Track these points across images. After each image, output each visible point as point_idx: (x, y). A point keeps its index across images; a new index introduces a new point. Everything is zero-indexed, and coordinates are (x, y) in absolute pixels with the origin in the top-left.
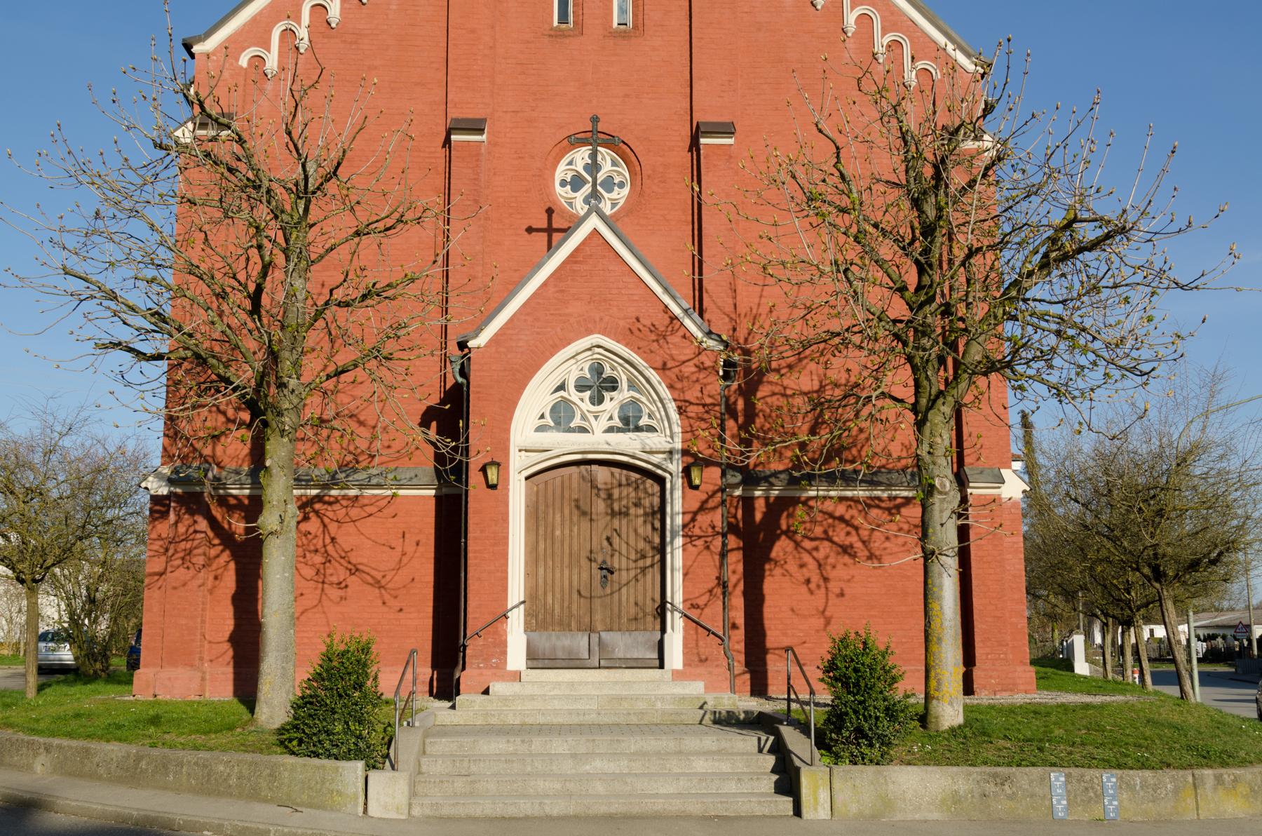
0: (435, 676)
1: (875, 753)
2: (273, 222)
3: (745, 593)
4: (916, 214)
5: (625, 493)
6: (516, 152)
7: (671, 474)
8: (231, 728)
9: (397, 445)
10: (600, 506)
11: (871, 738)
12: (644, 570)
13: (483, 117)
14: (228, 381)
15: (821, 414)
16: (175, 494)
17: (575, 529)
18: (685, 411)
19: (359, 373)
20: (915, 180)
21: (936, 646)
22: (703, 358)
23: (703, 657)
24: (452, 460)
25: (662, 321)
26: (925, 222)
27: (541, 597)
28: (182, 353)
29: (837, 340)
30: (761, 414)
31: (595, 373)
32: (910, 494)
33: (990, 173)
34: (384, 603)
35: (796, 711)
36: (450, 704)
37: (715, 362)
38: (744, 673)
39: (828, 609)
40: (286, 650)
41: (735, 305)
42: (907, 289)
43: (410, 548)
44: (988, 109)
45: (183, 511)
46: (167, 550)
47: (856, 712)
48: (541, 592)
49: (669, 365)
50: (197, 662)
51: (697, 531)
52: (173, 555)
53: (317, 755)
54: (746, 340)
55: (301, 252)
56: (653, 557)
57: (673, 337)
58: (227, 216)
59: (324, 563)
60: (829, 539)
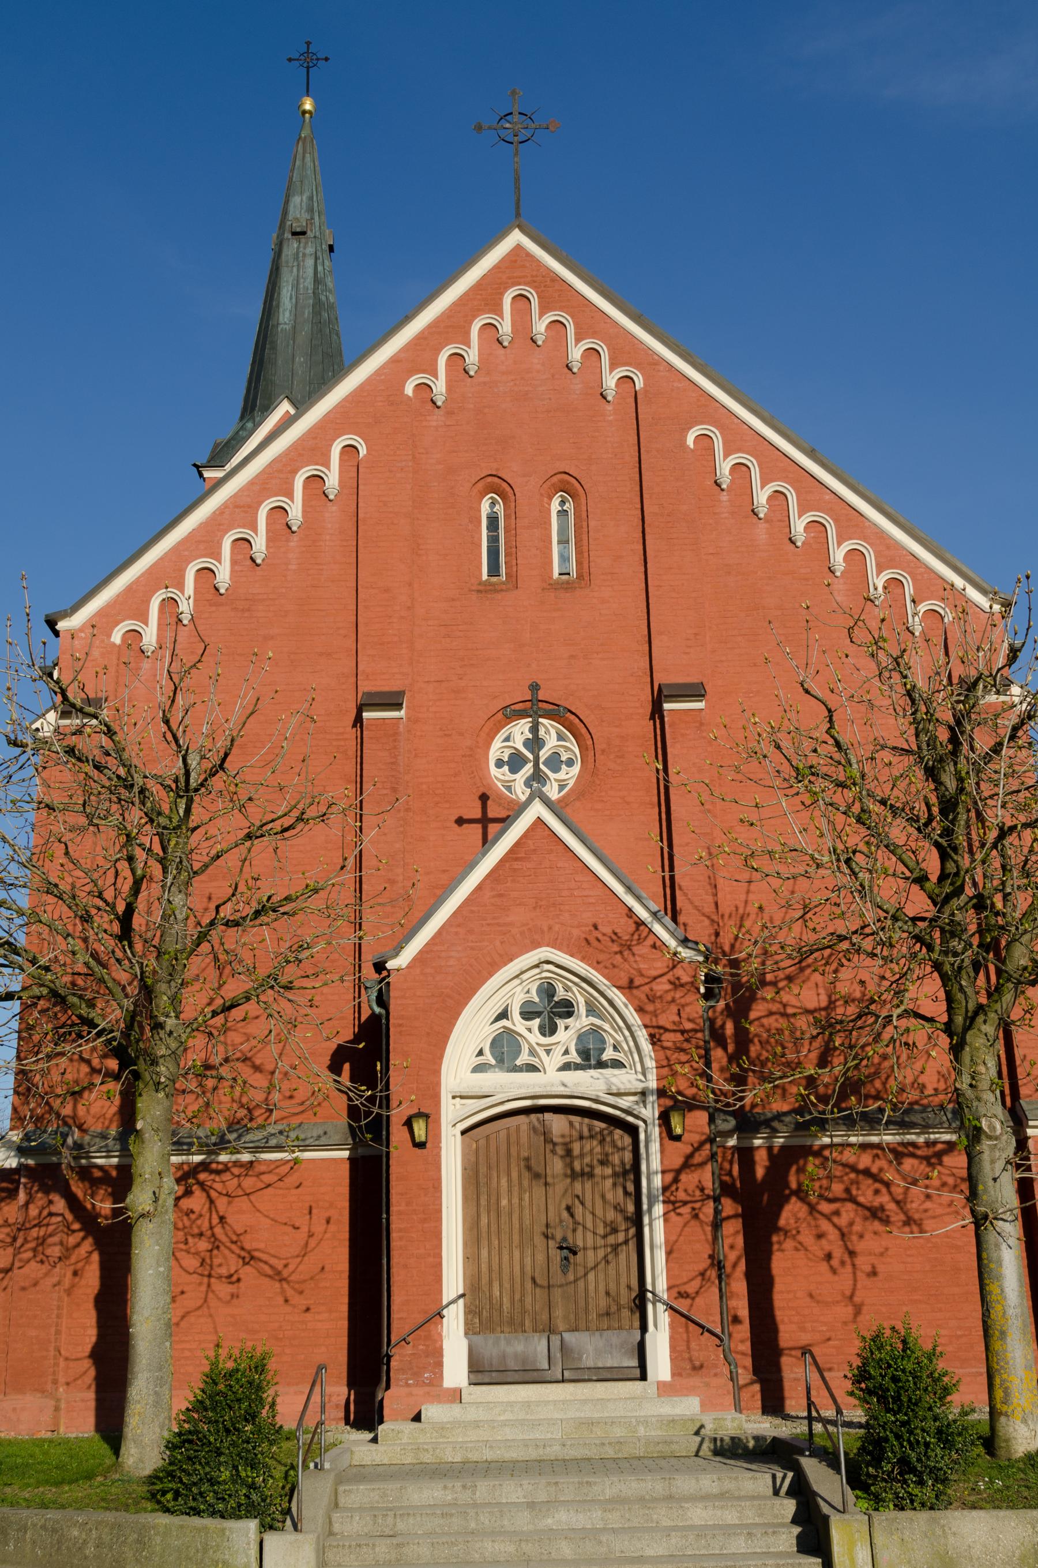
0: (352, 1397)
1: (928, 1493)
2: (148, 827)
3: (749, 1275)
4: (932, 786)
5: (587, 1148)
6: (441, 729)
7: (645, 1122)
8: (89, 1476)
9: (300, 1096)
10: (557, 1166)
11: (921, 1473)
12: (615, 1248)
13: (402, 689)
14: (92, 1024)
15: (831, 1039)
16: (26, 1167)
17: (527, 1196)
18: (659, 1040)
19: (251, 1008)
20: (928, 745)
21: (1000, 1342)
22: (679, 972)
23: (697, 1363)
24: (368, 1114)
25: (625, 928)
26: (944, 796)
27: (486, 1289)
28: (36, 991)
29: (845, 945)
30: (756, 1040)
31: (544, 996)
32: (954, 1137)
33: (1020, 733)
34: (286, 1301)
35: (821, 1435)
36: (371, 1435)
37: (694, 976)
38: (752, 1383)
39: (857, 1293)
40: (160, 1369)
41: (716, 904)
42: (928, 879)
43: (319, 1228)
44: (1014, 654)
45: (35, 1188)
46: (15, 1239)
47: (898, 1437)
48: (485, 1280)
49: (637, 983)
50: (49, 1387)
51: (681, 1195)
52: (22, 1245)
53: (197, 1512)
54: (732, 946)
55: (181, 862)
56: (627, 1230)
57: (640, 947)
58: (91, 824)
59: (211, 1251)
60: (853, 1200)
